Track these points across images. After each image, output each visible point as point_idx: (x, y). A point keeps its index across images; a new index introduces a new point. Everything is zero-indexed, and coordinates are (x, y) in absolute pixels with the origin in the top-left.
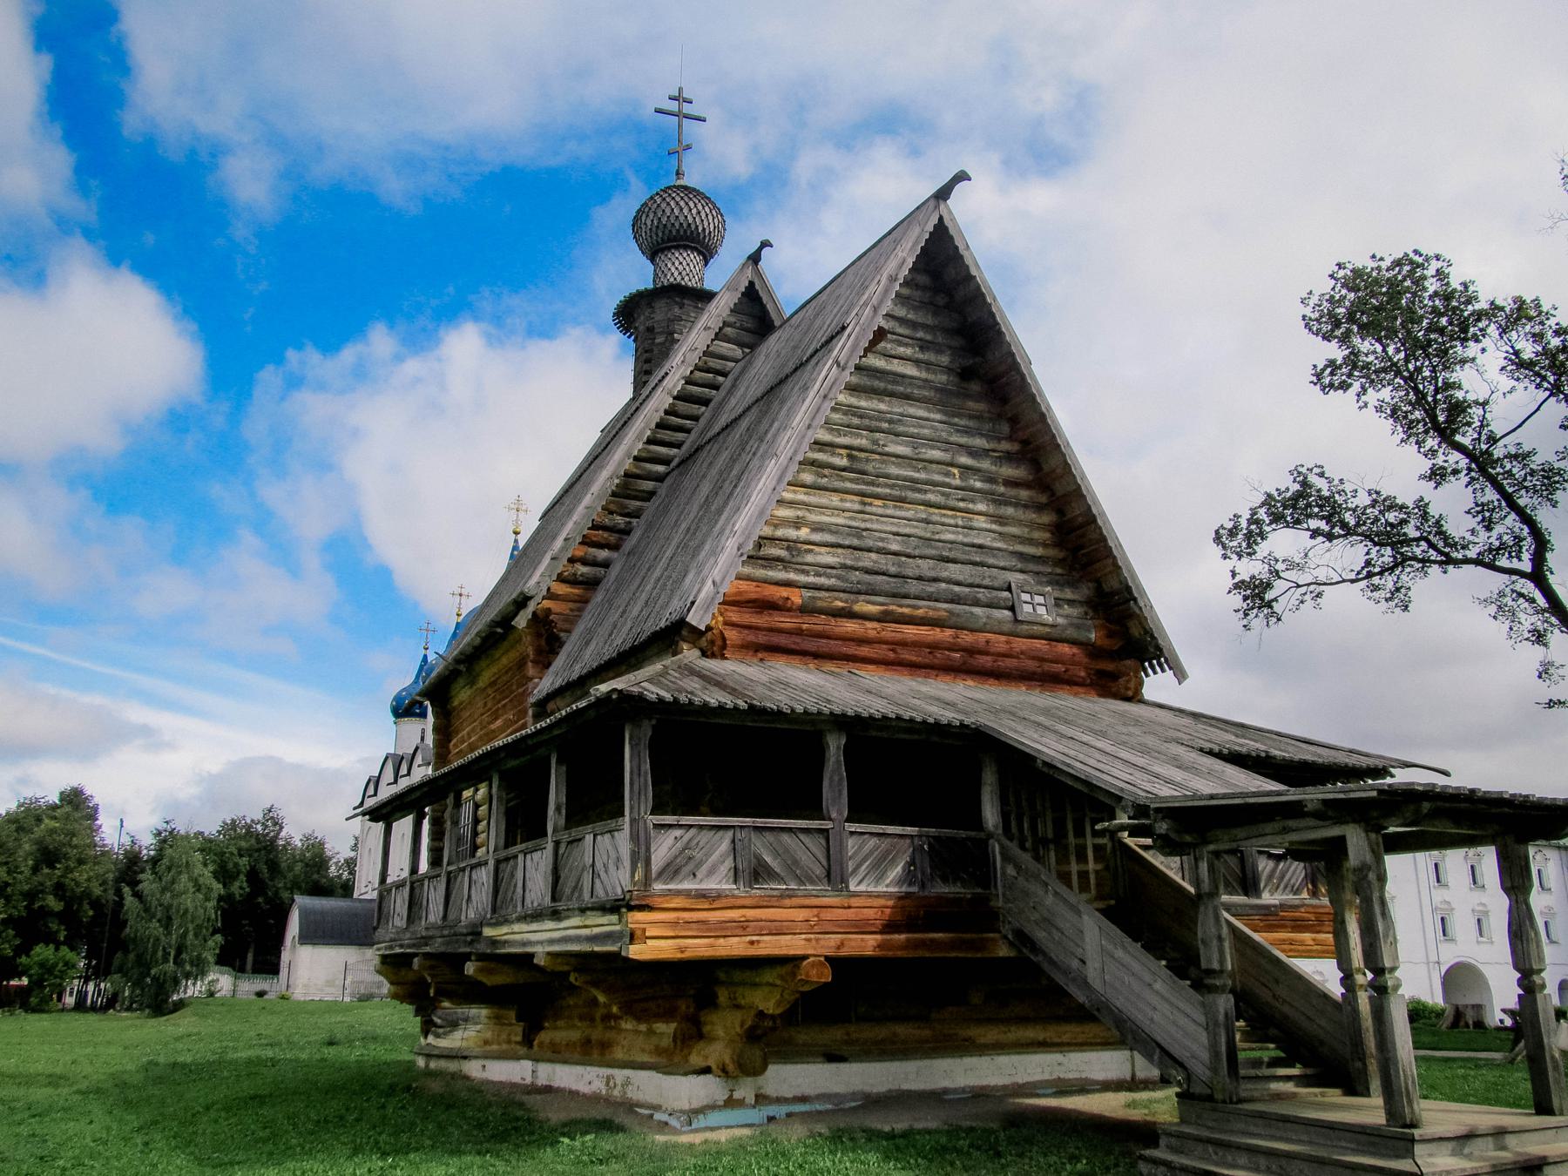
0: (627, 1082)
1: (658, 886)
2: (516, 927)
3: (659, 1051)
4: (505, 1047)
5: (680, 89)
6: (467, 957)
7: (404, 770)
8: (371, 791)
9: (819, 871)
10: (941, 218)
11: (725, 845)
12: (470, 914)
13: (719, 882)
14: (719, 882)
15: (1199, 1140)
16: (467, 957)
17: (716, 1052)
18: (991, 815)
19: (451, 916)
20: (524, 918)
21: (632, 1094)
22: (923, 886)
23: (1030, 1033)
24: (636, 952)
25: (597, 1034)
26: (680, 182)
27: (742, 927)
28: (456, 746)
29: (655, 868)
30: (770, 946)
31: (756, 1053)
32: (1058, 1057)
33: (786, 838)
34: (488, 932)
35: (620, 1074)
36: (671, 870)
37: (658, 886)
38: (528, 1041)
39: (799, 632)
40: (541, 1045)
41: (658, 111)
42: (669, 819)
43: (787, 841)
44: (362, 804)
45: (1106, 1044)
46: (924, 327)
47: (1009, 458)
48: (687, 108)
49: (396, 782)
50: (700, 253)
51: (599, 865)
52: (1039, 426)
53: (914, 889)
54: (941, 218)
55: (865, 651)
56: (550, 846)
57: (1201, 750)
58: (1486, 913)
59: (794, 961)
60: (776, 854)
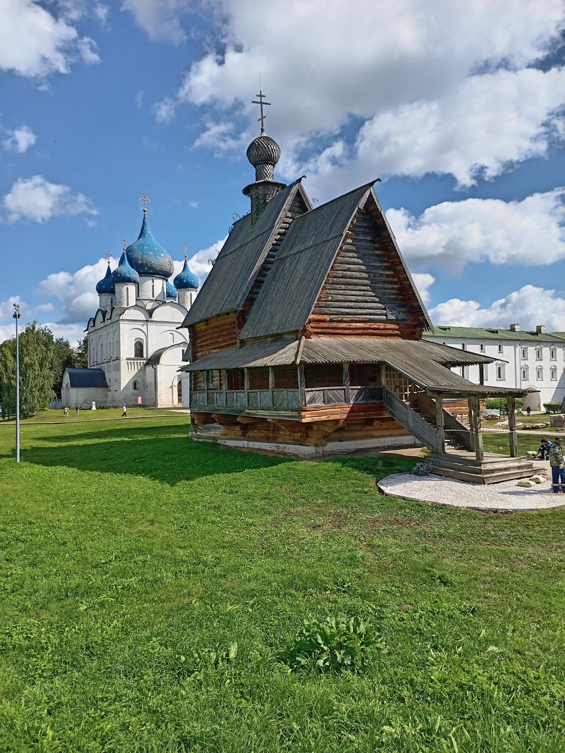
0: (285, 447)
1: (308, 406)
2: (259, 411)
3: (294, 440)
4: (234, 437)
5: (261, 92)
6: (237, 416)
7: (108, 316)
8: (91, 324)
9: (343, 399)
10: (371, 193)
11: (322, 394)
12: (237, 406)
13: (320, 404)
14: (320, 404)
15: (296, 265)
16: (237, 416)
17: (313, 441)
18: (384, 382)
19: (229, 404)
20: (260, 409)
21: (286, 450)
22: (367, 401)
23: (387, 433)
24: (304, 421)
25: (271, 434)
26: (264, 134)
27: (326, 414)
28: (199, 343)
29: (307, 401)
30: (332, 417)
31: (324, 441)
32: (395, 438)
33: (335, 391)
34: (246, 411)
35: (282, 446)
36: (311, 402)
37: (308, 406)
38: (244, 435)
39: (328, 328)
40: (249, 437)
41: (253, 102)
42: (310, 389)
43: (337, 392)
44: (87, 330)
45: (408, 435)
46: (364, 227)
47: (387, 268)
48: (264, 100)
49: (104, 321)
50: (272, 165)
51: (290, 399)
52: (395, 260)
53: (365, 402)
54: (371, 193)
55: (346, 331)
56: (271, 392)
57: (439, 362)
58: (541, 369)
59: (338, 421)
60: (333, 395)
